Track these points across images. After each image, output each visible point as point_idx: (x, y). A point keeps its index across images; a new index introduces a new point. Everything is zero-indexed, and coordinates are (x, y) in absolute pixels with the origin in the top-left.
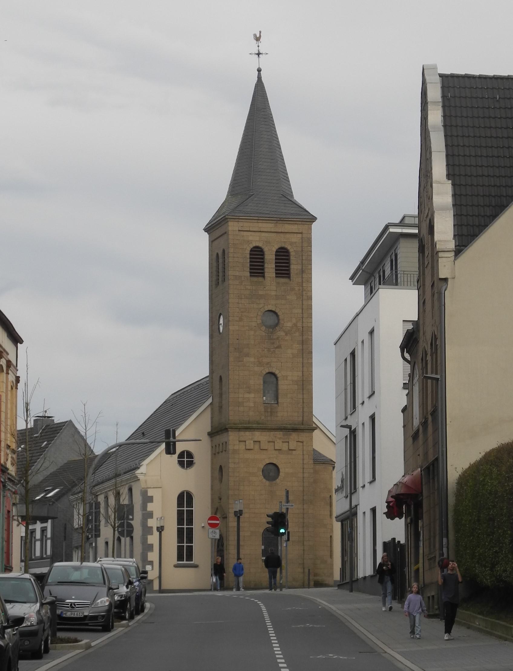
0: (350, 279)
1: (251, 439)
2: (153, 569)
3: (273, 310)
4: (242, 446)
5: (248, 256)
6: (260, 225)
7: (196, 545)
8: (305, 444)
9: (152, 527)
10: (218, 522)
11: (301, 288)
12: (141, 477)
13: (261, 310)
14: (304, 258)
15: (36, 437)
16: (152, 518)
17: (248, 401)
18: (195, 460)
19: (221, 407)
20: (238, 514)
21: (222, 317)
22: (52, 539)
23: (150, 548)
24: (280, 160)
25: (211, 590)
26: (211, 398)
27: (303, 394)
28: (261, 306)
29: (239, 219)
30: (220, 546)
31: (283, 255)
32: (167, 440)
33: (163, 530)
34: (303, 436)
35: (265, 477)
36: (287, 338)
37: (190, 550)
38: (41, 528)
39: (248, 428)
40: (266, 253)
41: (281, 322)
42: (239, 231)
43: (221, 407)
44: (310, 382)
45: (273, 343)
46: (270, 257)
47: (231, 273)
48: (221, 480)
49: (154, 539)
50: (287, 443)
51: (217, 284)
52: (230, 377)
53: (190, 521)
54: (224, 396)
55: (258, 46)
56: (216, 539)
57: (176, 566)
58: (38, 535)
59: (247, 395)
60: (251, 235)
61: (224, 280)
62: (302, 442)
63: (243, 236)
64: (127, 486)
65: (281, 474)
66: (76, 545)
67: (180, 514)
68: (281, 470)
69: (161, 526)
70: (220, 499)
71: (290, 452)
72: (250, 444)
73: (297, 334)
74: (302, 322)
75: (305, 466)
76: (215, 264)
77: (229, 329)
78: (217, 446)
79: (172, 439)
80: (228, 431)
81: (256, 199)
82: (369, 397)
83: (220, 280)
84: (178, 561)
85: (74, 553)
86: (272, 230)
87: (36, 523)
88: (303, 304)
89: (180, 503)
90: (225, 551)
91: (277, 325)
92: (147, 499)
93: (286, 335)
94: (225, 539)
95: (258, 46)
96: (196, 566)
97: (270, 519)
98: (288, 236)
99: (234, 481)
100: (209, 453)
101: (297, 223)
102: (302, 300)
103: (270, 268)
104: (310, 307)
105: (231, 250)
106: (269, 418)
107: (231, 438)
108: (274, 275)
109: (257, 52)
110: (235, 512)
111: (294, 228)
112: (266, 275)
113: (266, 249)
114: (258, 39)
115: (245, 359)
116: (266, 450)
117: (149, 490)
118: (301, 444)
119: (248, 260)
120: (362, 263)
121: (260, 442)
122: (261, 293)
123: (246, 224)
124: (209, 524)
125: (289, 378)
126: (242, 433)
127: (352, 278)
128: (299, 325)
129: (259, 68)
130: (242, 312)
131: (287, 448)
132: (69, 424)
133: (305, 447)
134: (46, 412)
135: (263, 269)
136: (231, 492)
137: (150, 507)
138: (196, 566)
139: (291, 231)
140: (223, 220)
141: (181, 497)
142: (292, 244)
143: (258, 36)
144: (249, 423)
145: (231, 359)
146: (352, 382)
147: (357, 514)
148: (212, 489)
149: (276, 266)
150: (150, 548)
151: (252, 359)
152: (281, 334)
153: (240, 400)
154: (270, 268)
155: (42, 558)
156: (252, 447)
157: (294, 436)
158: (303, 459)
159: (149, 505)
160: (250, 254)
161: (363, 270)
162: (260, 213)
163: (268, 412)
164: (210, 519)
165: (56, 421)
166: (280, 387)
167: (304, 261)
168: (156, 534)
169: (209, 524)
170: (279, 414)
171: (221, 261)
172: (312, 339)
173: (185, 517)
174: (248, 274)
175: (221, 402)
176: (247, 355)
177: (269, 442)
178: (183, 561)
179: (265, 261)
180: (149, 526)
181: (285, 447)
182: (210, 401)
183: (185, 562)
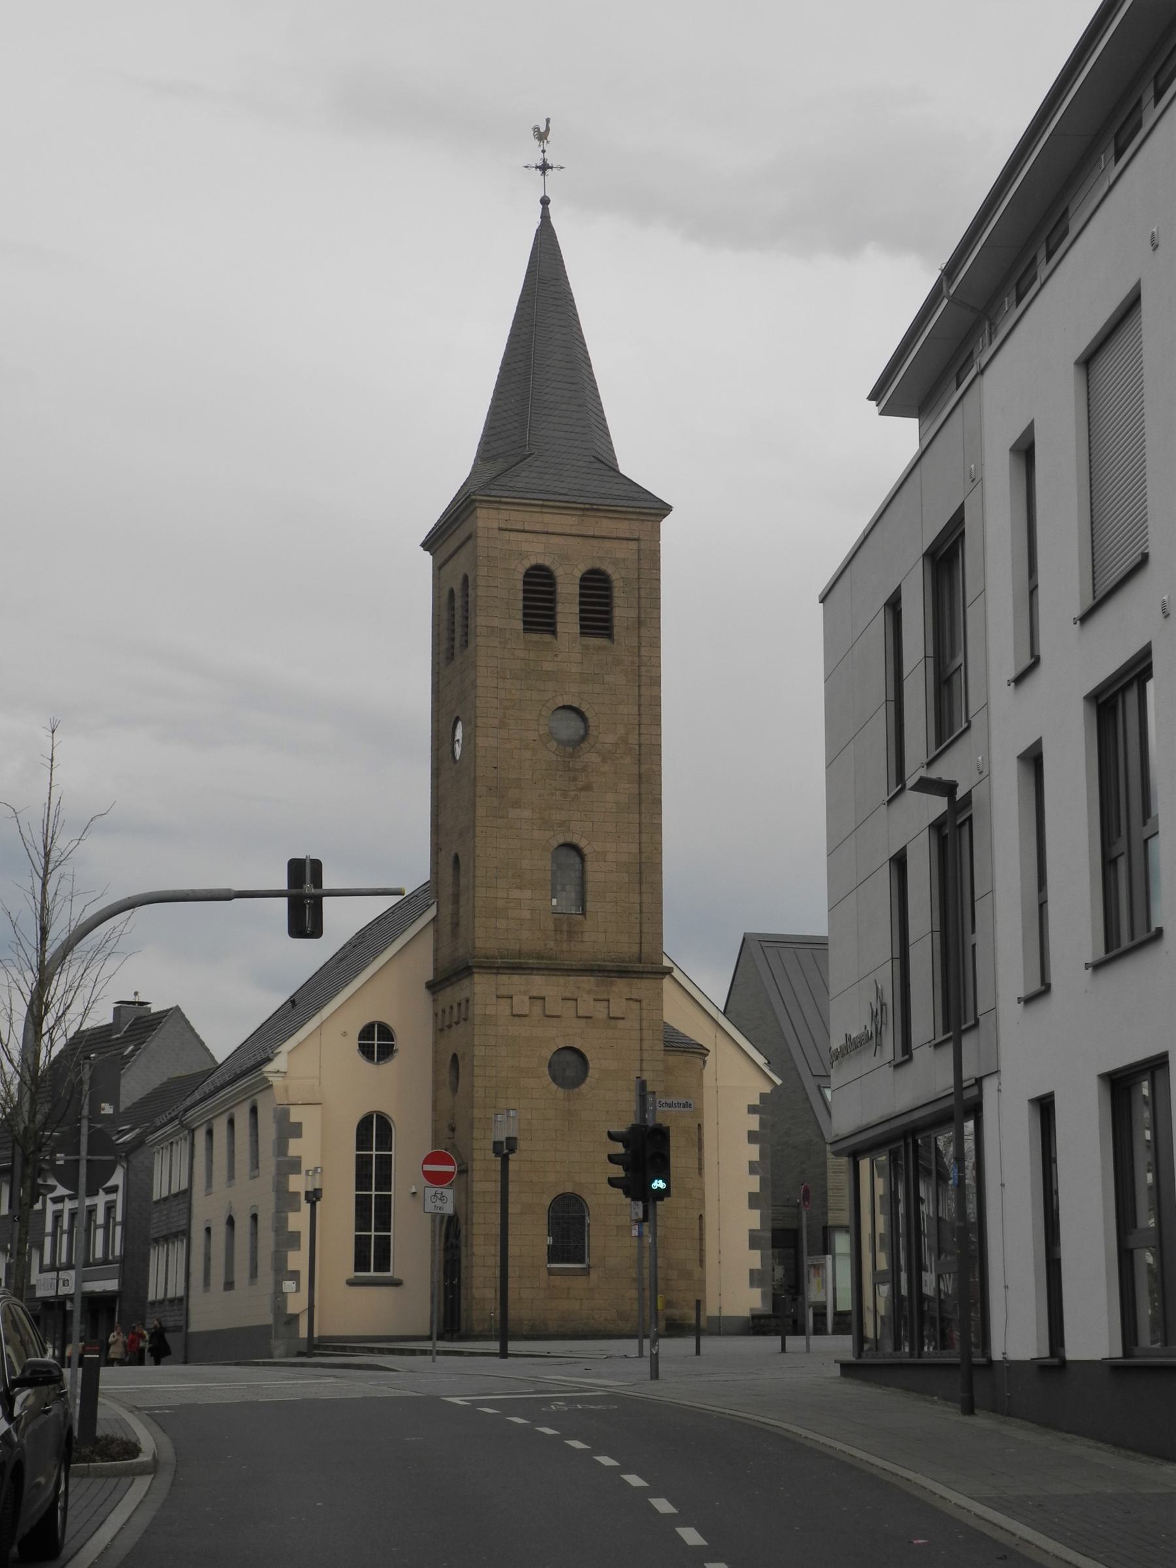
0: (870, 398)
2: (298, 1290)
3: (576, 705)
4: (504, 1008)
5: (520, 586)
6: (547, 518)
7: (398, 1233)
8: (644, 1004)
9: (297, 1194)
10: (450, 1169)
12: (275, 1080)
14: (643, 593)
15: (117, 1039)
16: (299, 1172)
17: (516, 908)
18: (398, 1043)
19: (456, 925)
20: (505, 1150)
21: (460, 725)
22: (124, 1223)
23: (293, 1240)
24: (589, 387)
25: (429, 1338)
26: (434, 907)
27: (641, 893)
29: (500, 502)
30: (451, 1235)
31: (596, 587)
32: (294, 891)
33: (318, 1199)
34: (641, 988)
35: (554, 1079)
37: (384, 1246)
38: (107, 1203)
40: (559, 580)
41: (593, 732)
42: (500, 529)
43: (456, 925)
44: (656, 866)
47: (481, 622)
48: (455, 1089)
49: (298, 1221)
50: (606, 1003)
51: (451, 657)
52: (478, 852)
53: (385, 1181)
54: (463, 900)
55: (544, 151)
56: (443, 1216)
57: (351, 1283)
58: (100, 1218)
59: (515, 894)
61: (466, 644)
62: (640, 1001)
64: (249, 1101)
65: (591, 1072)
66: (156, 1236)
67: (362, 1164)
68: (591, 1065)
69: (315, 1190)
70: (453, 1130)
71: (613, 1022)
72: (522, 1004)
75: (646, 1056)
76: (445, 615)
77: (475, 744)
78: (448, 1010)
79: (308, 888)
80: (471, 974)
81: (537, 463)
82: (1019, 680)
83: (457, 644)
84: (356, 1270)
85: (152, 1251)
86: (574, 532)
87: (97, 1194)
88: (640, 696)
90: (463, 1248)
91: (584, 738)
92: (289, 1130)
93: (604, 760)
94: (462, 1221)
95: (544, 151)
96: (397, 1283)
97: (619, 1148)
98: (607, 544)
99: (485, 1088)
100: (429, 1030)
101: (628, 516)
102: (639, 686)
103: (568, 612)
104: (656, 701)
105: (483, 571)
107: (478, 989)
108: (577, 629)
109: (540, 163)
110: (497, 1146)
111: (622, 528)
112: (560, 628)
113: (559, 572)
114: (542, 136)
115: (513, 813)
116: (558, 1017)
117: (293, 1109)
118: (635, 1005)
119: (521, 595)
120: (949, 272)
121: (544, 998)
122: (548, 666)
124: (427, 1174)
126: (504, 979)
127: (875, 395)
128: (633, 739)
129: (545, 196)
131: (605, 1016)
132: (175, 1013)
133: (645, 1014)
134: (136, 994)
135: (553, 617)
136: (477, 1113)
137: (295, 1147)
138: (397, 1283)
139: (614, 535)
140: (462, 511)
141: (364, 1126)
143: (543, 129)
144: (520, 954)
145: (480, 812)
146: (892, 696)
147: (1167, 1063)
148: (434, 1109)
149: (581, 611)
150: (293, 1240)
151: (527, 813)
152: (592, 758)
153: (501, 904)
154: (568, 612)
155: (105, 1261)
156: (526, 1011)
157: (621, 986)
160: (525, 583)
161: (952, 300)
162: (547, 492)
163: (561, 932)
164: (429, 1160)
165: (155, 1008)
166: (590, 877)
167: (643, 601)
168: (306, 1207)
169: (427, 1174)
171: (458, 603)
172: (660, 770)
173: (373, 1172)
174: (520, 625)
175: (456, 914)
176: (517, 804)
178: (369, 1270)
179: (559, 598)
180: (291, 1189)
181: (600, 1011)
182: (431, 913)
183: (372, 1273)
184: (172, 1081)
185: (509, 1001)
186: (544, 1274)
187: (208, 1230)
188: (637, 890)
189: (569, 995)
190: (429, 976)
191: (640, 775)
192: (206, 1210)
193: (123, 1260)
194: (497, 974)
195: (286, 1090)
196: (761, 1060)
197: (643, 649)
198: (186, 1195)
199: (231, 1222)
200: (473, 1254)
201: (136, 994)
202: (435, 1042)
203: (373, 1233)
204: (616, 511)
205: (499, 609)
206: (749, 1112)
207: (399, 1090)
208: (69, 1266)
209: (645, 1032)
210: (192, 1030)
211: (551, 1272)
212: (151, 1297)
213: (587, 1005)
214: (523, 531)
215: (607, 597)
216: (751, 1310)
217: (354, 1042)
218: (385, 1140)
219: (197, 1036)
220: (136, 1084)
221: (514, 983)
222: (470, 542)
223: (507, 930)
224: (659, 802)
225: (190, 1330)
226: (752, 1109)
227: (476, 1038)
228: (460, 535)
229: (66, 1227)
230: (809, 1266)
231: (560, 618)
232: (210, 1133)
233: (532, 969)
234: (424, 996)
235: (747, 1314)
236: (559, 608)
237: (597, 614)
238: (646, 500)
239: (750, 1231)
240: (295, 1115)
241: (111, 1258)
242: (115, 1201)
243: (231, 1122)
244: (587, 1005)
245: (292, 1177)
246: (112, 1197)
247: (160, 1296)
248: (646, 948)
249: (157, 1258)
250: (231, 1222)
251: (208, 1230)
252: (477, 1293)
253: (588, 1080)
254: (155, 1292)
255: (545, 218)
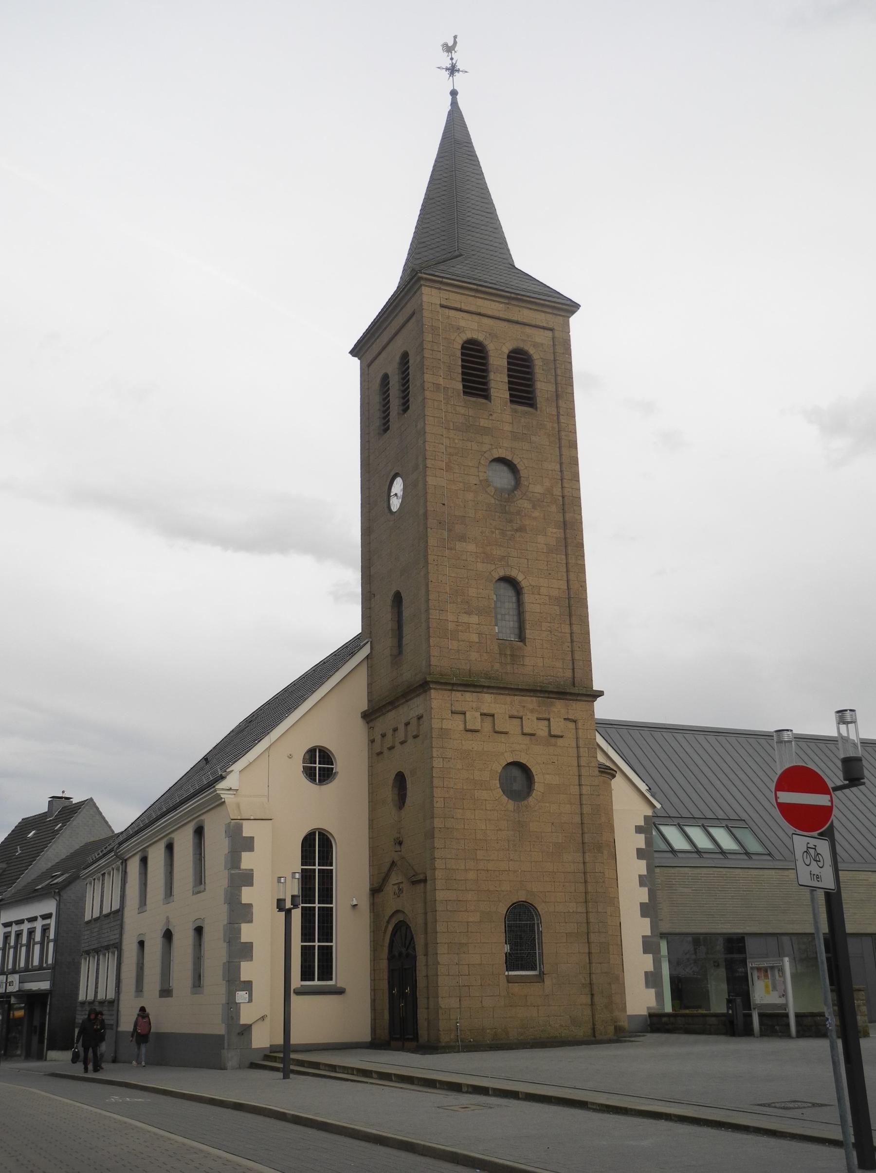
1: (477, 709)
3: (509, 458)
4: (455, 724)
5: (459, 354)
6: (480, 302)
8: (580, 725)
11: (556, 425)
12: (227, 797)
13: (486, 455)
17: (463, 631)
18: (339, 766)
22: (56, 941)
26: (368, 646)
27: (571, 624)
28: (485, 448)
29: (441, 283)
31: (520, 365)
36: (536, 514)
37: (327, 954)
38: (43, 926)
39: (470, 684)
40: (491, 353)
41: (524, 482)
42: (442, 306)
45: (511, 521)
46: (498, 362)
50: (546, 722)
53: (327, 895)
58: (38, 937)
59: (465, 618)
60: (463, 318)
61: (405, 407)
62: (575, 721)
63: (448, 317)
65: (537, 786)
66: (87, 949)
70: (400, 843)
71: (553, 740)
72: (474, 720)
73: (554, 508)
74: (562, 487)
75: (584, 772)
76: (376, 399)
84: (302, 980)
85: (83, 961)
86: (501, 315)
88: (561, 455)
89: (307, 856)
90: (421, 960)
96: (340, 992)
98: (528, 330)
103: (499, 382)
104: (575, 461)
106: (509, 667)
107: (435, 704)
111: (539, 318)
112: (493, 393)
113: (491, 347)
114: (449, 49)
115: (459, 546)
116: (506, 733)
118: (572, 725)
119: (460, 363)
121: (493, 716)
122: (483, 423)
123: (452, 296)
124: (787, 810)
125: (543, 591)
126: (457, 695)
130: (450, 454)
131: (546, 734)
133: (580, 732)
134: (63, 792)
137: (247, 861)
138: (340, 992)
139: (534, 323)
141: (308, 842)
142: (535, 345)
145: (432, 542)
148: (371, 827)
151: (471, 547)
154: (499, 382)
155: (41, 968)
156: (477, 726)
157: (559, 707)
158: (578, 757)
159: (245, 855)
165: (75, 801)
166: (528, 607)
167: (559, 378)
169: (787, 810)
170: (527, 661)
176: (463, 538)
177: (511, 717)
178: (314, 980)
181: (541, 729)
182: (366, 651)
183: (316, 982)
184: (87, 845)
185: (462, 716)
186: (503, 981)
187: (141, 944)
188: (568, 622)
189: (516, 713)
190: (364, 706)
191: (565, 522)
192: (134, 924)
193: (54, 967)
194: (452, 690)
195: (238, 806)
196: (643, 787)
197: (561, 417)
198: (118, 915)
199: (168, 935)
200: (438, 963)
201: (63, 792)
202: (371, 767)
203: (317, 944)
204: (536, 304)
205: (441, 377)
206: (636, 832)
207: (341, 809)
208: (14, 972)
209: (581, 750)
210: (100, 813)
211: (509, 980)
212: (81, 997)
213: (532, 724)
214: (461, 310)
215: (528, 373)
216: (648, 1008)
217: (298, 765)
218: (326, 857)
219: (103, 818)
220: (60, 849)
221: (467, 700)
222: (413, 320)
223: (458, 651)
224: (581, 546)
225: (120, 1029)
226: (639, 830)
227: (434, 750)
228: (408, 311)
229: (12, 943)
230: (752, 968)
231: (492, 384)
232: (144, 861)
233: (484, 687)
234: (360, 725)
235: (645, 1012)
236: (492, 376)
237: (523, 392)
238: (558, 298)
239: (643, 937)
240: (248, 830)
241: (45, 965)
242: (49, 925)
243: (170, 847)
244: (532, 724)
245: (245, 890)
246: (47, 921)
247: (91, 997)
248: (579, 674)
249: (87, 969)
250: (168, 935)
251: (141, 944)
252: (443, 1003)
253: (534, 794)
254: (85, 993)
255: (454, 103)
